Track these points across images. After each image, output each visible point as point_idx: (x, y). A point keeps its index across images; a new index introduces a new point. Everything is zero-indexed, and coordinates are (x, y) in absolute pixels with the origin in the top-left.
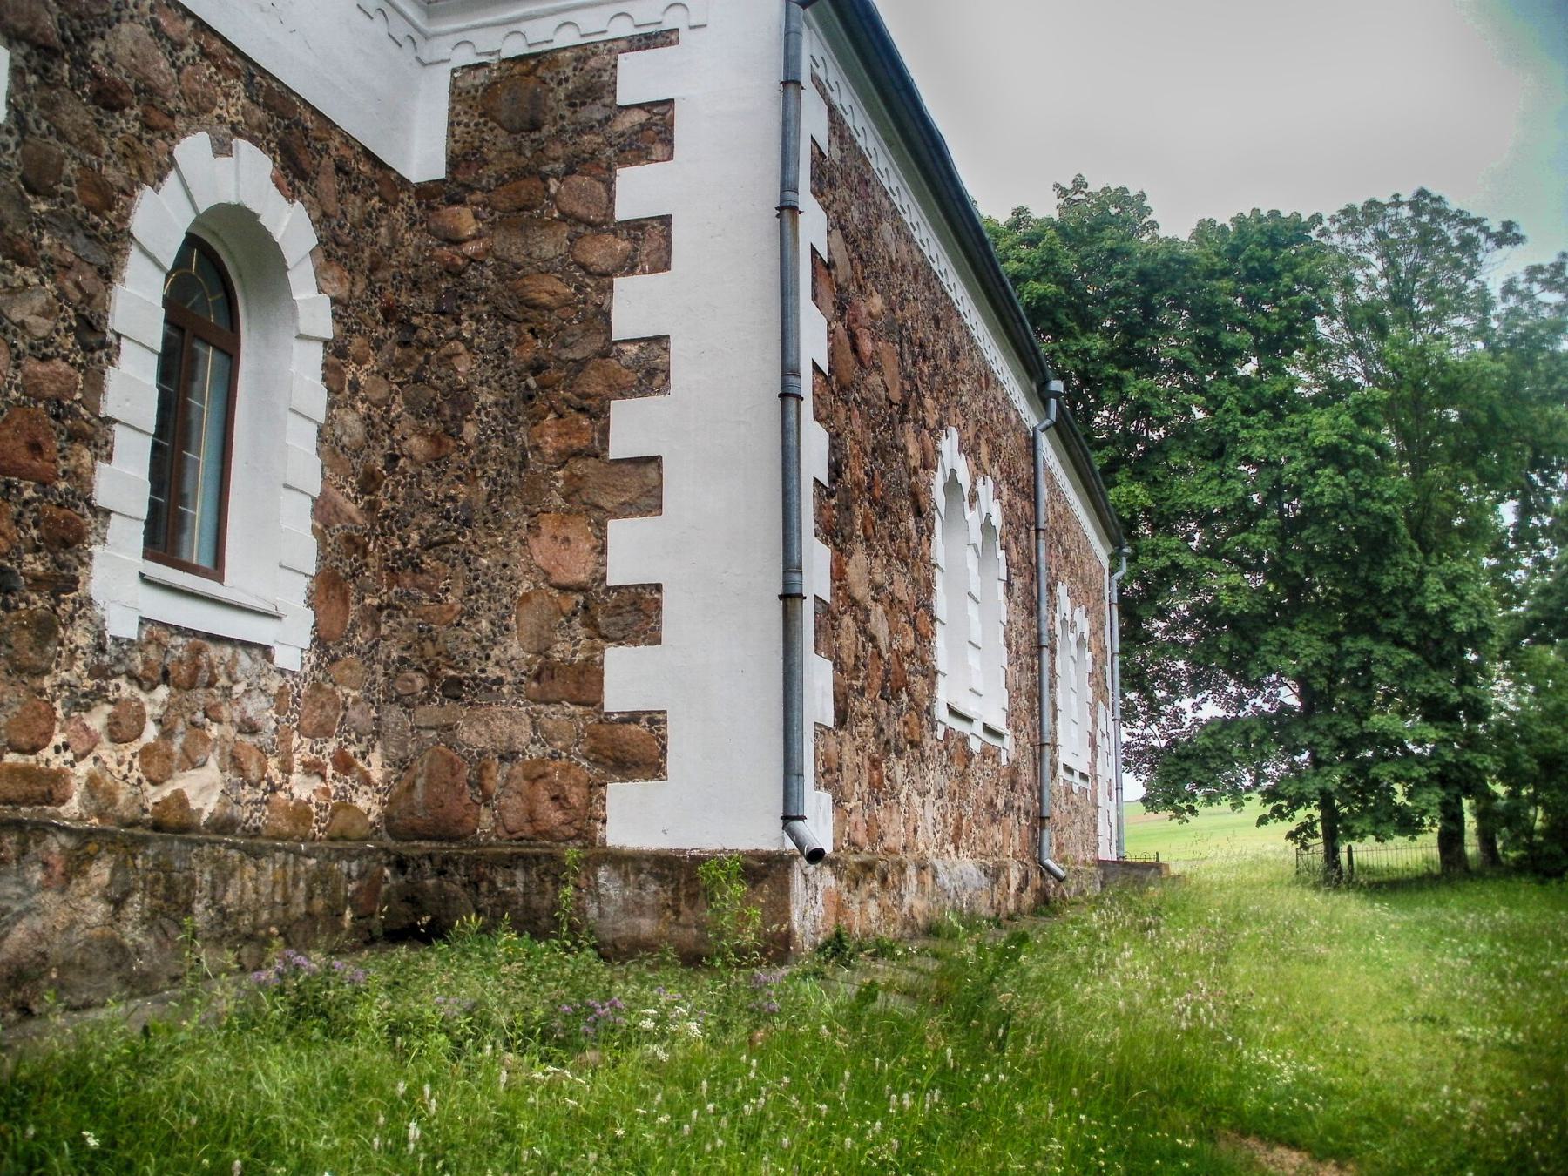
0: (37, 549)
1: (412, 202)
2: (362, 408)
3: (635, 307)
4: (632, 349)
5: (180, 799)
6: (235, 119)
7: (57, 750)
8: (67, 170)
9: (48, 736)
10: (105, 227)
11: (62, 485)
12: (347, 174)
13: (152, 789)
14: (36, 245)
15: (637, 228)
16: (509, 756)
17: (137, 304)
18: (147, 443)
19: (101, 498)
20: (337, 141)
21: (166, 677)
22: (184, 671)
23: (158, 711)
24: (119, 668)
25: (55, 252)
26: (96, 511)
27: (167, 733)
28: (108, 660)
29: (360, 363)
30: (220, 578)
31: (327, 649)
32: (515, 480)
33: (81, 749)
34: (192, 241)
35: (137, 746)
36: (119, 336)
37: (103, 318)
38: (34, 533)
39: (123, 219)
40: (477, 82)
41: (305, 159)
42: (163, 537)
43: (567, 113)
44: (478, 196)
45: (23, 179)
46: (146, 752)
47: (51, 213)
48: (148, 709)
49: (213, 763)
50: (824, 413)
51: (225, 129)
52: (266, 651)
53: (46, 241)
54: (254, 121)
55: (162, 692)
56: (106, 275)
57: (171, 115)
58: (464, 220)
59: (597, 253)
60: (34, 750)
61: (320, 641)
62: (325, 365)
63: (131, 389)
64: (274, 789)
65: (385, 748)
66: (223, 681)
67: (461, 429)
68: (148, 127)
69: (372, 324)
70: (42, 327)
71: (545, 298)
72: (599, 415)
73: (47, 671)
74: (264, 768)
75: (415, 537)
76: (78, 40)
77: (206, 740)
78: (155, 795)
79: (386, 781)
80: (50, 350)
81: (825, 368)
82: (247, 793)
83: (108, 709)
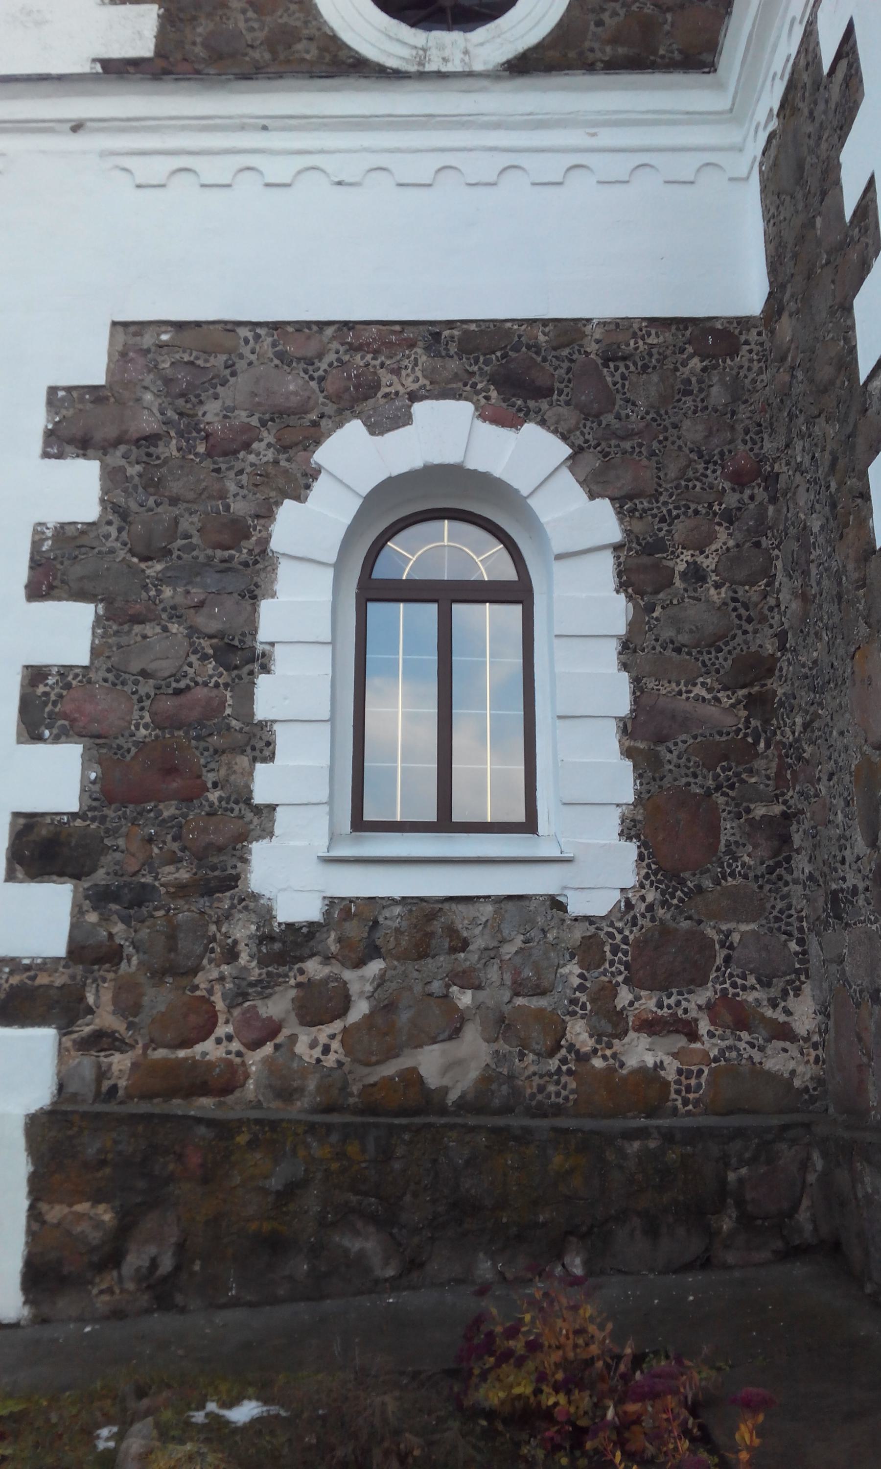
5: (412, 1078)
7: (219, 1041)
26: (258, 810)
39: (267, 540)
48: (354, 989)
55: (375, 967)
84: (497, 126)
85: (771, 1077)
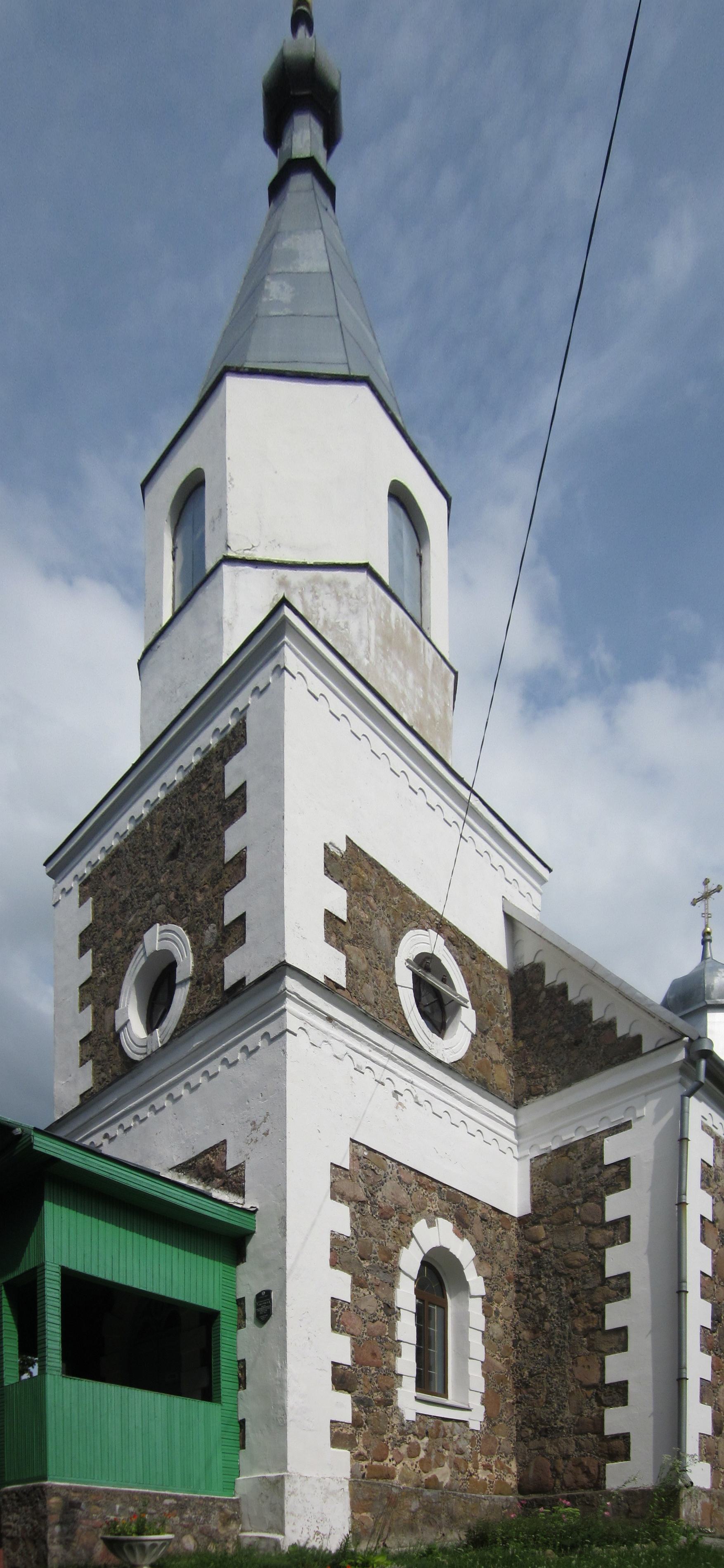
0: (378, 1391)
1: (517, 1227)
2: (501, 1322)
3: (616, 1261)
4: (614, 1282)
5: (435, 1478)
6: (435, 1210)
8: (374, 1248)
9: (387, 1455)
10: (390, 1267)
11: (385, 1367)
12: (486, 1221)
13: (424, 1475)
14: (366, 1280)
15: (615, 1223)
16: (566, 1457)
17: (405, 1296)
18: (414, 1348)
19: (399, 1370)
20: (480, 1206)
21: (427, 1434)
22: (434, 1432)
23: (425, 1447)
24: (410, 1431)
25: (373, 1281)
27: (428, 1453)
28: (406, 1429)
29: (498, 1303)
30: (446, 1397)
31: (491, 1421)
32: (567, 1344)
33: (399, 1460)
34: (424, 1263)
35: (418, 1459)
36: (399, 1309)
37: (393, 1302)
38: (377, 1385)
39: (396, 1262)
40: (542, 1164)
41: (467, 1219)
42: (423, 1382)
43: (582, 1172)
44: (545, 1219)
45: (359, 1255)
46: (421, 1461)
47: (370, 1266)
49: (446, 1464)
50: (708, 1294)
51: (432, 1215)
52: (466, 1422)
53: (370, 1277)
54: (443, 1208)
55: (426, 1439)
56: (393, 1285)
57: (410, 1215)
58: (540, 1231)
59: (597, 1237)
60: (382, 1460)
61: (488, 1417)
62: (483, 1307)
63: (406, 1329)
64: (471, 1475)
65: (517, 1459)
66: (449, 1435)
67: (543, 1325)
68: (401, 1222)
69: (502, 1285)
70: (371, 1310)
71: (576, 1263)
72: (601, 1313)
73: (385, 1433)
74: (467, 1467)
75: (526, 1373)
76: (372, 1194)
77: (444, 1457)
78: (425, 1476)
79: (518, 1472)
80: (375, 1318)
81: (709, 1272)
82: (460, 1476)
83: (407, 1446)
84: (459, 1099)
85: (506, 1483)
